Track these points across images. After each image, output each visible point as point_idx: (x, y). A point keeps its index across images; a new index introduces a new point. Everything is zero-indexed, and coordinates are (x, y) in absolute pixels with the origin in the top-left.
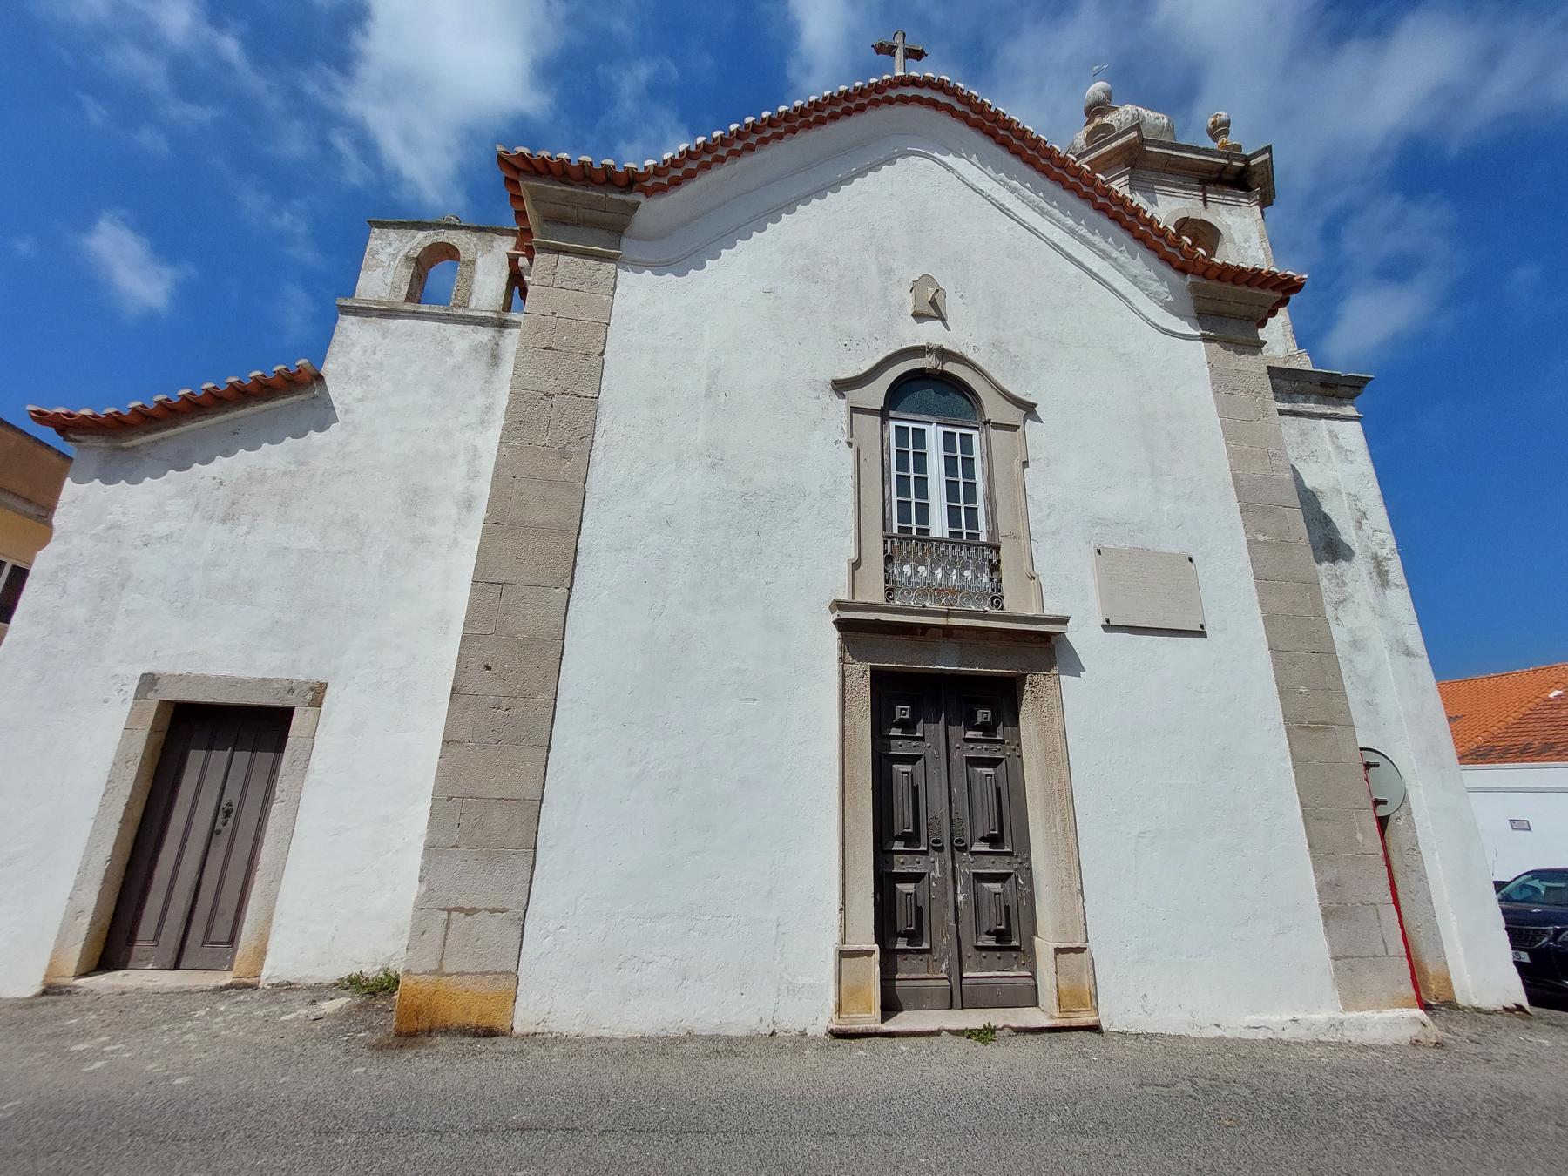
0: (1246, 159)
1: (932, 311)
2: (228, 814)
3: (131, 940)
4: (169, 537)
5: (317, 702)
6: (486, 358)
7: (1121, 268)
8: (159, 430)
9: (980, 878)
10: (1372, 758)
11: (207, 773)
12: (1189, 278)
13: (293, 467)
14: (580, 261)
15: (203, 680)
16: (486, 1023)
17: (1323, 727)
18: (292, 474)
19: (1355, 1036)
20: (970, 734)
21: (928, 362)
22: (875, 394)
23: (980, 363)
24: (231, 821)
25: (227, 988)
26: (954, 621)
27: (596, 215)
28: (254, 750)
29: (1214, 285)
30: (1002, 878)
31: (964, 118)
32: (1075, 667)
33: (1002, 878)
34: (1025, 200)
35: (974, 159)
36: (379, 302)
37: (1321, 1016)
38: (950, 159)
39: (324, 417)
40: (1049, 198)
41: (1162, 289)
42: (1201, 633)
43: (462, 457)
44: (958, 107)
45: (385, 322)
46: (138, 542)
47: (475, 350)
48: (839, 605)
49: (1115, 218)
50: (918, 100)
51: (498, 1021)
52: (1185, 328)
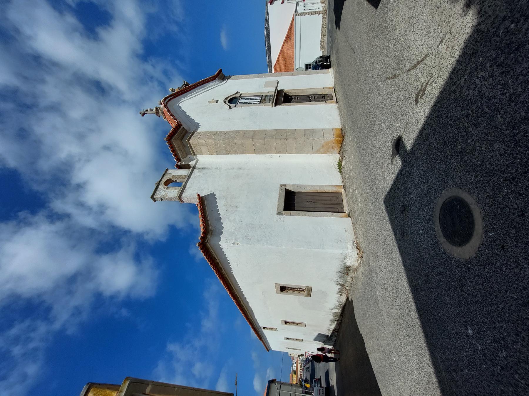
4: (240, 217)
5: (285, 185)
7: (211, 86)
25: (345, 190)
31: (174, 97)
33: (315, 97)
39: (213, 195)
40: (195, 91)
41: (217, 82)
45: (186, 188)
48: (273, 107)
49: (203, 84)
50: (168, 102)
52: (224, 82)
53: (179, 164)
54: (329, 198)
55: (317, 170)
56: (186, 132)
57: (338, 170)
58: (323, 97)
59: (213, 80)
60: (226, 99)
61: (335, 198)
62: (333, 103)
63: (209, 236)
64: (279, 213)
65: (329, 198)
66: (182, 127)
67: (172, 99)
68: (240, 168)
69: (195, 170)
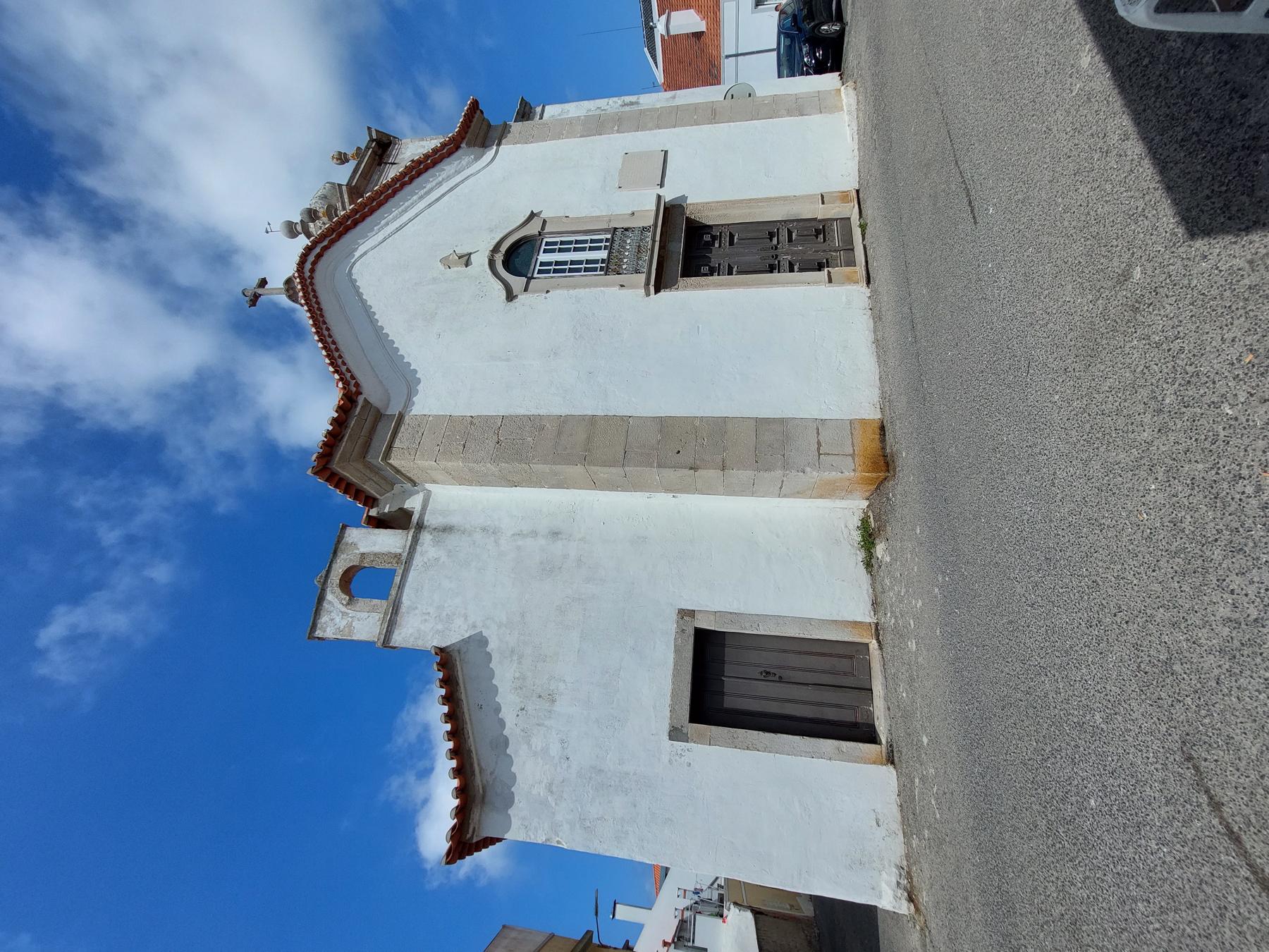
0: (372, 140)
1: (466, 260)
2: (768, 673)
3: (855, 725)
4: (562, 741)
5: (692, 613)
6: (445, 535)
7: (449, 178)
8: (472, 765)
9: (790, 240)
10: (729, 96)
11: (739, 690)
12: (463, 145)
13: (515, 658)
14: (402, 429)
15: (674, 695)
16: (878, 431)
17: (714, 112)
18: (521, 657)
19: (854, 107)
20: (717, 245)
21: (499, 258)
22: (517, 282)
23: (501, 235)
24: (772, 671)
25: (879, 642)
26: (658, 238)
27: (368, 425)
28: (723, 662)
29: (468, 135)
30: (790, 233)
31: (332, 242)
32: (684, 198)
33: (790, 233)
34: (395, 219)
35: (361, 241)
36: (385, 614)
37: (846, 118)
38: (357, 254)
39: (479, 641)
42: (666, 152)
43: (520, 543)
44: (325, 243)
45: (403, 609)
46: (565, 766)
47: (437, 543)
48: (648, 294)
50: (314, 263)
51: (877, 425)
53: (373, 512)
54: (824, 663)
55: (790, 561)
56: (379, 416)
57: (861, 555)
58: (818, 232)
59: (450, 154)
60: (496, 249)
61: (844, 664)
62: (850, 280)
63: (475, 815)
64: (675, 734)
65: (824, 663)
66: (361, 400)
67: (326, 248)
68: (555, 534)
69: (426, 537)
